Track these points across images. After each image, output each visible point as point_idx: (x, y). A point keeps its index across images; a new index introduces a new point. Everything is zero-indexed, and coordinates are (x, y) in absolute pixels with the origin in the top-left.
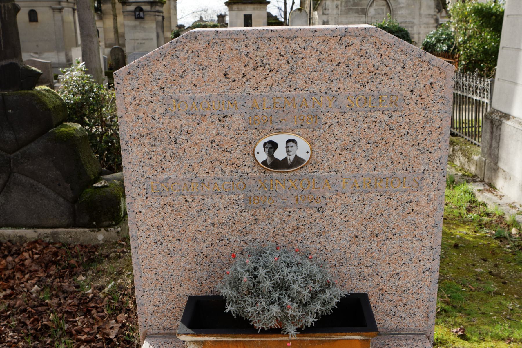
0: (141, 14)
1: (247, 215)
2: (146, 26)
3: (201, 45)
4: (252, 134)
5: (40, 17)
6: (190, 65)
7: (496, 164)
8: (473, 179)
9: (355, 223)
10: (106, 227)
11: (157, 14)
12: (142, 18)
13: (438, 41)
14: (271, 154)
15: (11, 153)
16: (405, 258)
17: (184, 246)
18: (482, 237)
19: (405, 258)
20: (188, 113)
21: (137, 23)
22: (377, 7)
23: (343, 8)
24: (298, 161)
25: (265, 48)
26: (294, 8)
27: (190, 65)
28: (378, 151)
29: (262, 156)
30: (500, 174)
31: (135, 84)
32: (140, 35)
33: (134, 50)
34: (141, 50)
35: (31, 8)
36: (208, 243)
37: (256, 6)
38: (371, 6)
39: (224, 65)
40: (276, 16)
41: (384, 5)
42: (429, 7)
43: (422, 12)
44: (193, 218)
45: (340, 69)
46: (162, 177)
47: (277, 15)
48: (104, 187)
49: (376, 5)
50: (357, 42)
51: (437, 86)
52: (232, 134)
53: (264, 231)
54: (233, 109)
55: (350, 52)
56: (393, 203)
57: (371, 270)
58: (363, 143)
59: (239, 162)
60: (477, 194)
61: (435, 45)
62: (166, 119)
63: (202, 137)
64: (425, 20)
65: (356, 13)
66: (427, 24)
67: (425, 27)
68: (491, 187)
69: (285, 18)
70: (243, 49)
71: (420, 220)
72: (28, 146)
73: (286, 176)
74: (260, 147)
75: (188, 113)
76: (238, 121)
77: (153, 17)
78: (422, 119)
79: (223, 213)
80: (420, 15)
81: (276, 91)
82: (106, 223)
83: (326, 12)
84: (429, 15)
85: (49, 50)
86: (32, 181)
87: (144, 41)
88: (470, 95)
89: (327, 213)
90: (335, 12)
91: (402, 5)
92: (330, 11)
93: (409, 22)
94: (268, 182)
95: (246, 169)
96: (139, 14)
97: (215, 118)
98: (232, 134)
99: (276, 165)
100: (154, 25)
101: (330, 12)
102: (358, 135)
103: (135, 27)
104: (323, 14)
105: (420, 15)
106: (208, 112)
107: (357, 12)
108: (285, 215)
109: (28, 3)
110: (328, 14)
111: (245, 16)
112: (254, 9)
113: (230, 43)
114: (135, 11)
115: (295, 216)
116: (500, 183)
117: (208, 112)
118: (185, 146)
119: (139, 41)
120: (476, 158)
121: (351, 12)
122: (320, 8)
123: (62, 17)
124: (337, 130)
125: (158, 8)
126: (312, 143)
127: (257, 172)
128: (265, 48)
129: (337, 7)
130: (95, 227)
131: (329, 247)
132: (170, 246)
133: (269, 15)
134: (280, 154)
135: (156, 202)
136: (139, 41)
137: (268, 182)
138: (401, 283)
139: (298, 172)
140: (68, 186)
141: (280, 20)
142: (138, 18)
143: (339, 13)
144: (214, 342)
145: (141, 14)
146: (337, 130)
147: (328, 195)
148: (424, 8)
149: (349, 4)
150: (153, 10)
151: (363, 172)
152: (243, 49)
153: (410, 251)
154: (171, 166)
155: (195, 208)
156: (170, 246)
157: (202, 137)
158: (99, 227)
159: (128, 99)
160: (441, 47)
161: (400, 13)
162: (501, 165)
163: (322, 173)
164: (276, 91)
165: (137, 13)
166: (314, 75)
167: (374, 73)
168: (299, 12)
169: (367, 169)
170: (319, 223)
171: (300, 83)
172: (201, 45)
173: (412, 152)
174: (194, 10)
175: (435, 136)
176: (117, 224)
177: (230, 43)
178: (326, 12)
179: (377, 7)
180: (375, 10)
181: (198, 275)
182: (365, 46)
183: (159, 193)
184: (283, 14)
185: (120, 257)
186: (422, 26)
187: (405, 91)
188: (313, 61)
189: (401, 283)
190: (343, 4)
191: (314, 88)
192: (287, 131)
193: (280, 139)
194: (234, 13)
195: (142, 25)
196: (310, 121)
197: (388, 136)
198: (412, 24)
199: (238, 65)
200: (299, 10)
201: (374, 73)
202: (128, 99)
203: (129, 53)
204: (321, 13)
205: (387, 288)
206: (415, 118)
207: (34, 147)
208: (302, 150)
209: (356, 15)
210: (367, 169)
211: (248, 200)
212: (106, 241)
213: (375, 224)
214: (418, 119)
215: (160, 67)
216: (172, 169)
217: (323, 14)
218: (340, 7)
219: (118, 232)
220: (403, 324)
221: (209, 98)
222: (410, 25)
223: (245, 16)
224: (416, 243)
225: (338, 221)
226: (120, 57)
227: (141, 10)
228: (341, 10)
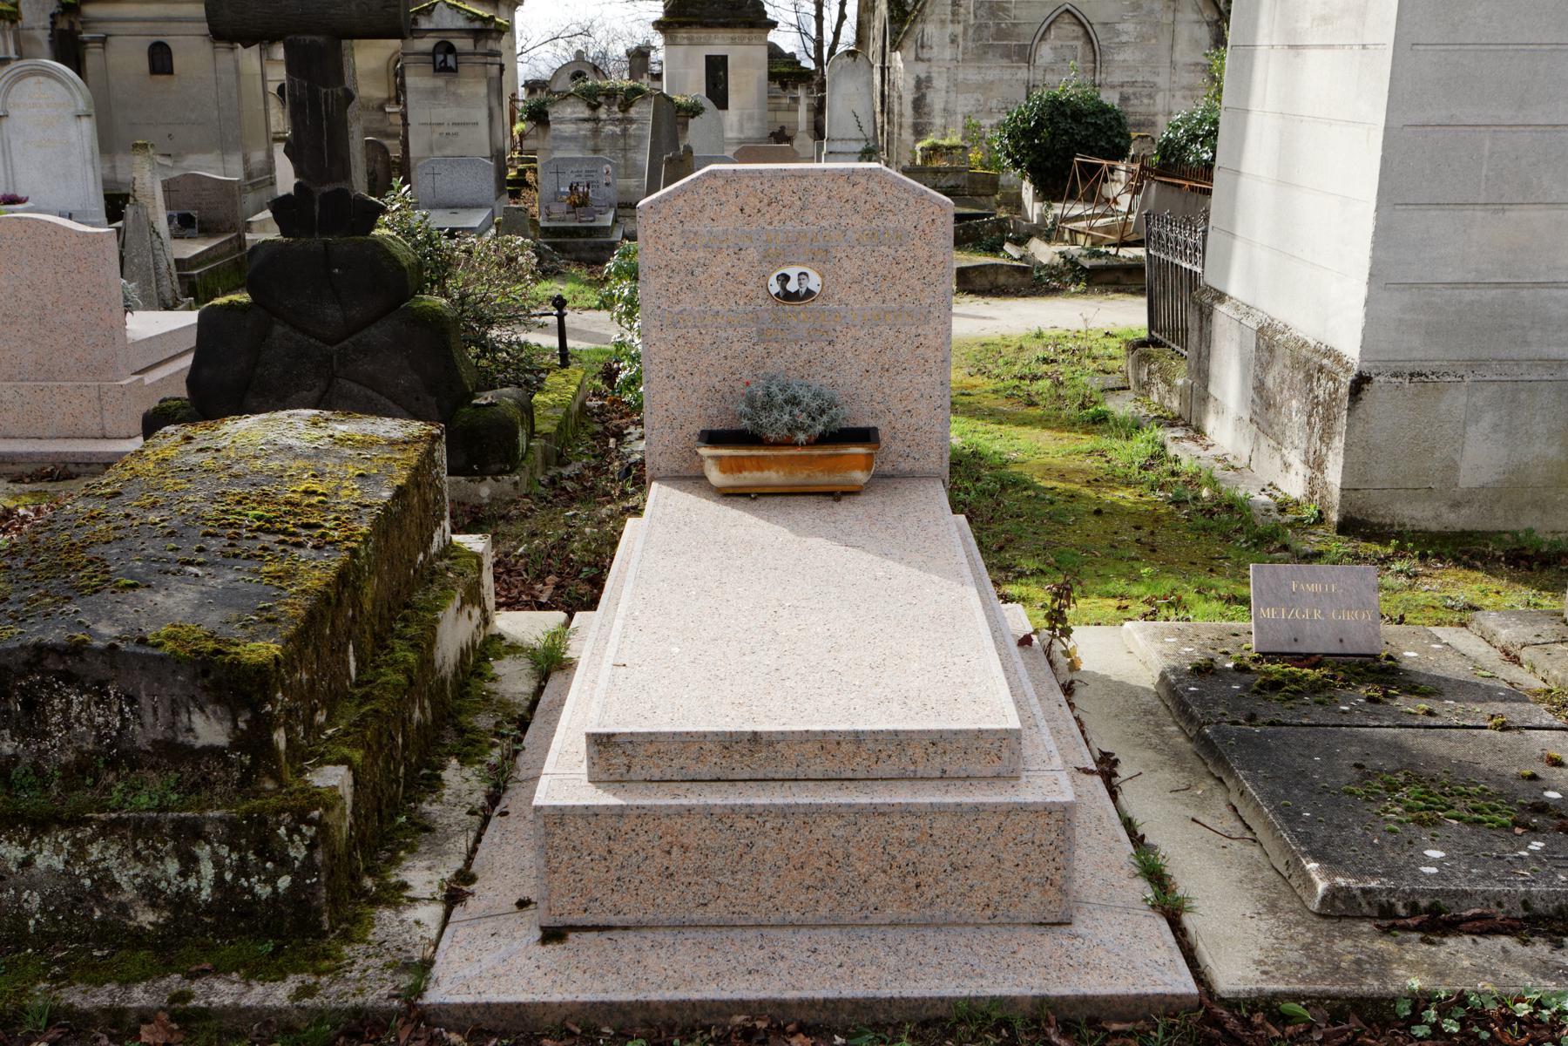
0: (451, 61)
1: (760, 348)
2: (461, 91)
3: (720, 182)
4: (766, 267)
5: (178, 62)
6: (708, 200)
7: (1206, 388)
8: (1173, 422)
9: (865, 357)
10: (495, 475)
11: (489, 59)
12: (454, 70)
13: (1193, 138)
14: (783, 288)
15: (332, 345)
16: (916, 395)
17: (696, 379)
18: (1149, 503)
19: (916, 395)
20: (705, 246)
21: (439, 82)
22: (1058, 43)
23: (970, 44)
24: (809, 293)
25: (779, 186)
26: (840, 49)
27: (708, 200)
28: (886, 285)
29: (775, 288)
30: (1211, 406)
31: (657, 218)
32: (449, 113)
33: (431, 150)
34: (448, 152)
35: (155, 39)
36: (720, 377)
37: (738, 33)
38: (1043, 38)
39: (740, 201)
40: (792, 55)
41: (1077, 38)
42: (1196, 43)
43: (1177, 56)
44: (707, 352)
45: (848, 206)
46: (677, 308)
47: (794, 50)
48: (491, 404)
49: (1057, 37)
50: (863, 181)
51: (938, 222)
52: (746, 267)
53: (775, 365)
54: (748, 243)
55: (857, 191)
56: (902, 336)
57: (882, 407)
58: (871, 276)
59: (752, 295)
60: (1169, 444)
61: (1184, 148)
62: (684, 251)
63: (718, 270)
64: (1186, 78)
65: (1002, 56)
66: (1191, 88)
67: (1184, 98)
68: (1199, 432)
69: (819, 60)
70: (758, 186)
71: (929, 354)
72: (365, 332)
73: (798, 308)
74: (773, 279)
75: (705, 246)
76: (752, 254)
77: (479, 69)
78: (925, 254)
79: (736, 346)
80: (1173, 64)
81: (789, 226)
82: (495, 468)
83: (926, 54)
84: (1197, 64)
85: (203, 149)
86: (369, 392)
87: (456, 129)
88: (1177, 261)
89: (839, 346)
90: (948, 53)
91: (1124, 38)
92: (935, 49)
93: (1144, 84)
94: (781, 314)
95: (760, 301)
96: (445, 61)
97: (731, 251)
98: (746, 267)
99: (788, 297)
100: (482, 90)
101: (934, 53)
102: (865, 270)
103: (433, 93)
104: (918, 59)
105: (1173, 64)
106: (724, 245)
107: (1007, 54)
108: (797, 348)
109: (148, 25)
110: (929, 60)
111: (708, 57)
112: (733, 42)
113: (746, 181)
114: (434, 53)
115: (806, 349)
116: (1211, 424)
117: (724, 245)
118: (702, 277)
119: (444, 129)
120: (1179, 382)
121: (990, 56)
122: (909, 44)
123: (236, 62)
124: (846, 264)
125: (491, 45)
126: (823, 276)
127: (770, 305)
128: (779, 186)
129: (953, 41)
130: (475, 473)
131: (840, 382)
132: (683, 380)
133: (774, 52)
134: (792, 286)
135: (670, 335)
136: (444, 129)
137: (781, 314)
138: (913, 421)
139: (810, 305)
140: (432, 400)
141: (803, 64)
142: (442, 69)
143: (960, 57)
144: (731, 457)
145: (451, 61)
146: (846, 264)
147: (838, 328)
148: (1182, 45)
149: (986, 33)
150: (479, 50)
151: (871, 305)
152: (758, 186)
153: (921, 387)
154: (686, 297)
155: (708, 340)
156: (683, 380)
157: (718, 270)
158: (482, 474)
159: (649, 232)
160: (1197, 154)
161: (1119, 58)
162: (1212, 389)
163: (833, 305)
164: (789, 226)
165: (440, 58)
166: (825, 211)
167: (880, 209)
168: (850, 60)
169: (876, 302)
170: (830, 357)
171: (812, 218)
172: (720, 182)
173: (918, 286)
174: (556, 31)
175: (939, 270)
176: (512, 471)
177: (746, 181)
178: (926, 54)
179: (1058, 43)
180: (1054, 49)
181: (710, 412)
182: (872, 185)
183: (674, 325)
184: (811, 45)
185: (526, 517)
186: (1179, 94)
187: (909, 226)
188: (823, 198)
189: (913, 421)
190: (970, 32)
191: (824, 223)
192: (799, 264)
193: (793, 272)
194: (680, 51)
195: (452, 89)
196: (821, 255)
197: (895, 269)
198: (1152, 89)
199: (753, 201)
200: (850, 53)
201: (880, 209)
202: (649, 232)
203: (419, 159)
204: (912, 56)
205: (898, 426)
206: (920, 253)
207: (376, 334)
208: (814, 282)
209: (1005, 62)
210: (876, 302)
211: (761, 332)
212: (493, 498)
213: (886, 358)
214: (923, 254)
215: (681, 202)
216: (688, 302)
217: (918, 59)
218: (960, 40)
219: (516, 483)
220: (917, 465)
221: (725, 232)
222: (1146, 91)
223: (708, 57)
224: (926, 378)
225: (849, 355)
226: (378, 166)
227: (450, 49)
228: (965, 48)
